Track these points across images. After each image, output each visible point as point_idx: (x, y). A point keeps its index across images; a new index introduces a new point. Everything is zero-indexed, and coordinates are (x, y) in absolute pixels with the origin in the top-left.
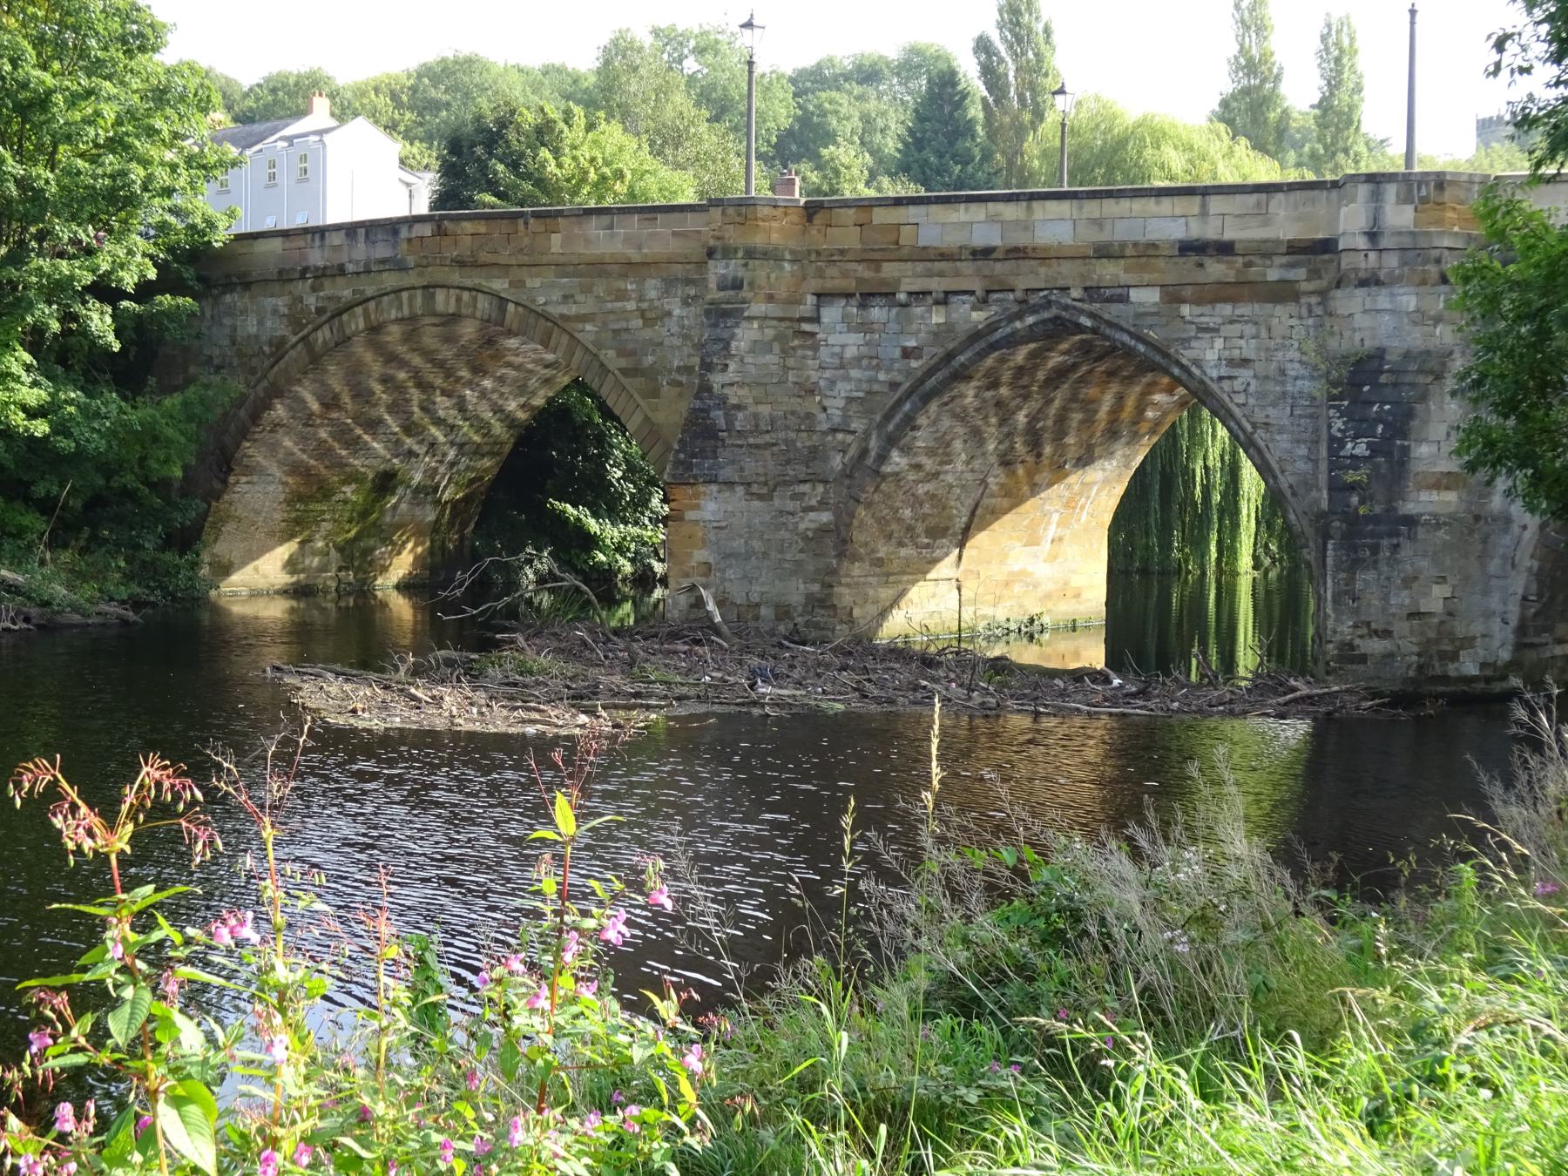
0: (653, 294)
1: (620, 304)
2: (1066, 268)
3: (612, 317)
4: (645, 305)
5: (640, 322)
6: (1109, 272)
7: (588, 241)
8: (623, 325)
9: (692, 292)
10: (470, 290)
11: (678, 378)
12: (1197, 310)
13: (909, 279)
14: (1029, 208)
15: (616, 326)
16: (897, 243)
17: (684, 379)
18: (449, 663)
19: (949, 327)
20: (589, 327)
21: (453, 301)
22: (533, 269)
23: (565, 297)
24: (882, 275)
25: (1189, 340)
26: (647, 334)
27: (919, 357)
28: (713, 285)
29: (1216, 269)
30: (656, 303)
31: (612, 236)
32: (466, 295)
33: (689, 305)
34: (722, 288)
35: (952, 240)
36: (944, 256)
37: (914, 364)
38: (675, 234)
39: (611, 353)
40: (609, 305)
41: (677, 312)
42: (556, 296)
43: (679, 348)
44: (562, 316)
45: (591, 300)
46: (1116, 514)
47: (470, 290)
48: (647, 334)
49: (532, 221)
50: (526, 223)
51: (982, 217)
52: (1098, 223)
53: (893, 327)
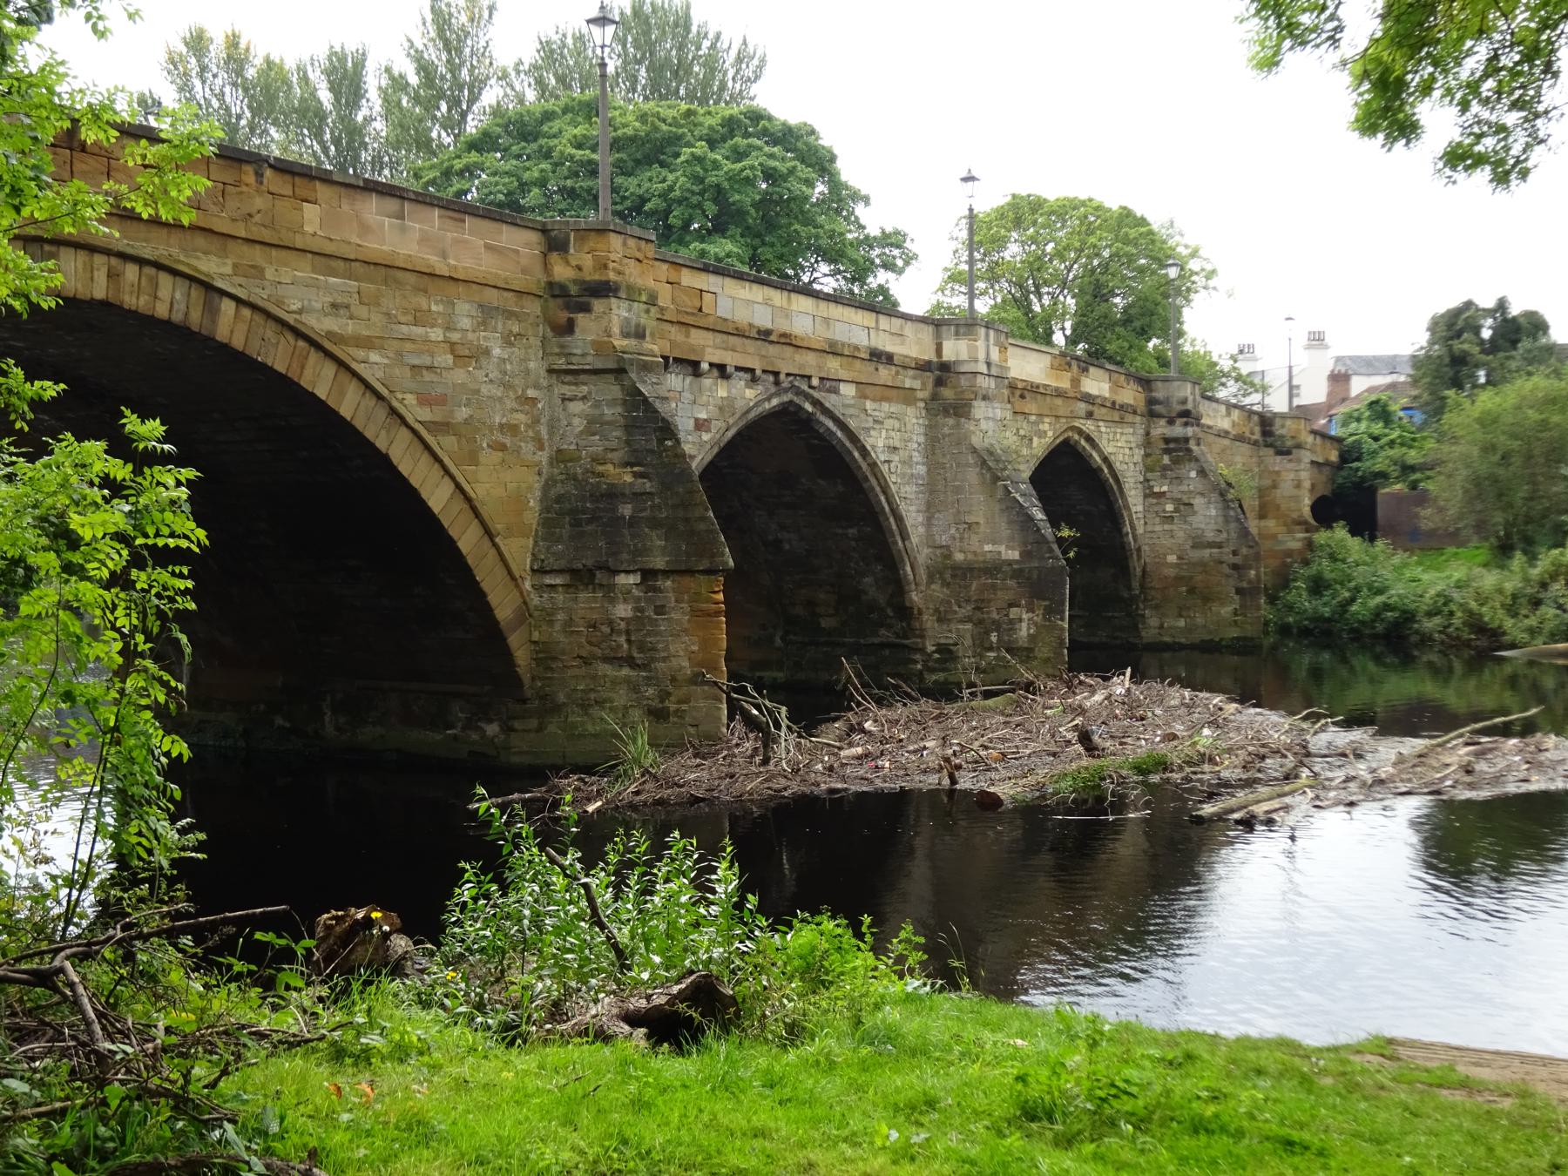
0: (465, 323)
1: (419, 330)
2: (811, 358)
3: (408, 346)
4: (455, 337)
5: (450, 359)
6: (833, 366)
7: (365, 229)
8: (427, 361)
9: (516, 329)
10: (141, 262)
11: (501, 438)
12: (875, 405)
13: (711, 350)
14: (789, 298)
15: (416, 362)
16: (700, 310)
17: (507, 441)
18: (302, 973)
19: (730, 400)
20: (374, 357)
21: (101, 277)
22: (274, 252)
23: (334, 306)
24: (691, 341)
25: (868, 429)
26: (459, 376)
27: (708, 431)
28: (616, 330)
29: (885, 374)
30: (470, 336)
31: (403, 229)
32: (131, 271)
33: (511, 344)
34: (625, 335)
35: (742, 316)
36: (739, 333)
37: (706, 437)
38: (488, 247)
39: (410, 399)
40: (405, 329)
41: (497, 351)
42: (320, 301)
43: (500, 399)
44: (330, 335)
45: (377, 318)
46: (404, 481)
47: (141, 262)
48: (459, 376)
49: (268, 173)
50: (259, 175)
51: (760, 299)
52: (826, 320)
53: (687, 396)
